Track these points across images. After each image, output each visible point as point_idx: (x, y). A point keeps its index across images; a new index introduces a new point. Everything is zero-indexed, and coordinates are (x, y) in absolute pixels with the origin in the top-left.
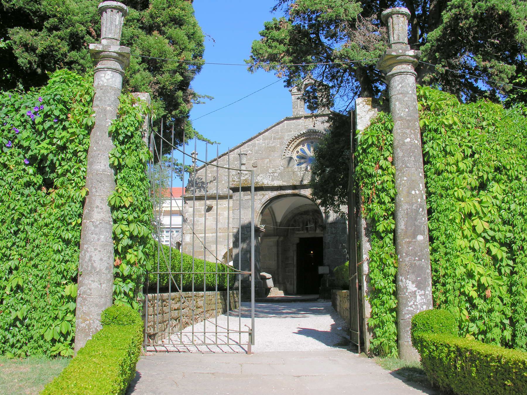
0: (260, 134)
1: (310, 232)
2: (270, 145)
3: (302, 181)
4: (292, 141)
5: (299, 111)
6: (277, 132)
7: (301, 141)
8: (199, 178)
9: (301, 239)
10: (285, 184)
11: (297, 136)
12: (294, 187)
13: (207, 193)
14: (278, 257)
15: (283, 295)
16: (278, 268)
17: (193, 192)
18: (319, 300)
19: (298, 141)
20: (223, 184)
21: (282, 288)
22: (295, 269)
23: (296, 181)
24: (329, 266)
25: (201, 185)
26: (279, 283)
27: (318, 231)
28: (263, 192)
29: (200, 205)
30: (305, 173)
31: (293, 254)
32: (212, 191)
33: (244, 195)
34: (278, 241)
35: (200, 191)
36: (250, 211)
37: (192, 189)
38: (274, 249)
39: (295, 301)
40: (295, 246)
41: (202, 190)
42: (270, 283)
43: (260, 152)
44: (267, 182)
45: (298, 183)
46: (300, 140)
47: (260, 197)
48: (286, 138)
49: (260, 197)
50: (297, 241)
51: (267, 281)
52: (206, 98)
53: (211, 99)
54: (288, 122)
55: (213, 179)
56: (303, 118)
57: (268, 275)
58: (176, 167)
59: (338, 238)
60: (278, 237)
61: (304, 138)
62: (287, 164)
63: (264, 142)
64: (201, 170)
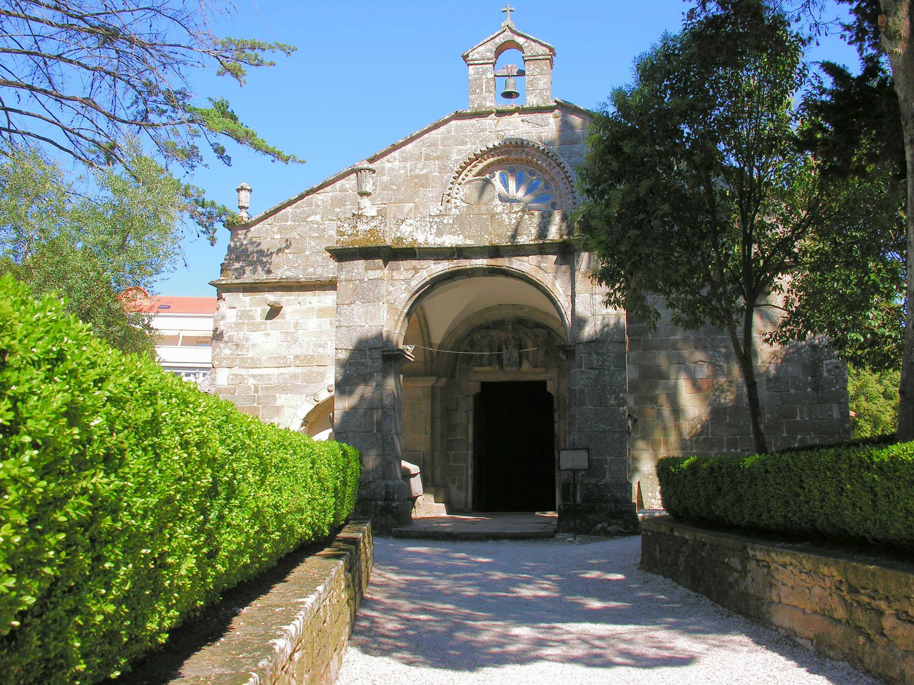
0: (395, 148)
1: (508, 369)
2: (417, 171)
3: (514, 236)
4: (464, 168)
5: (485, 99)
6: (433, 144)
7: (488, 166)
8: (252, 243)
9: (484, 385)
10: (469, 242)
11: (478, 152)
12: (495, 251)
13: (271, 276)
14: (433, 426)
15: (444, 514)
16: (433, 449)
17: (241, 272)
18: (559, 536)
19: (481, 166)
20: (307, 257)
21: (441, 497)
22: (471, 452)
23: (499, 236)
24: (587, 449)
25: (261, 258)
26: (434, 484)
27: (526, 366)
28: (414, 263)
29: (254, 305)
30: (521, 217)
31: (465, 419)
32: (283, 270)
33: (367, 269)
34: (433, 388)
35: (254, 271)
36: (382, 305)
37: (237, 265)
38: (425, 407)
39: (496, 537)
40: (471, 400)
41: (259, 269)
42: (416, 484)
43: (394, 187)
44: (425, 238)
45: (505, 242)
46: (485, 163)
47: (405, 275)
48: (454, 157)
49: (405, 275)
50: (476, 388)
51: (412, 479)
52: (277, 51)
53: (288, 51)
54: (459, 122)
55: (284, 245)
56: (493, 115)
57: (414, 468)
58: (200, 209)
59: (607, 378)
60: (435, 378)
61: (496, 158)
62: (475, 195)
63: (403, 164)
64: (258, 226)
